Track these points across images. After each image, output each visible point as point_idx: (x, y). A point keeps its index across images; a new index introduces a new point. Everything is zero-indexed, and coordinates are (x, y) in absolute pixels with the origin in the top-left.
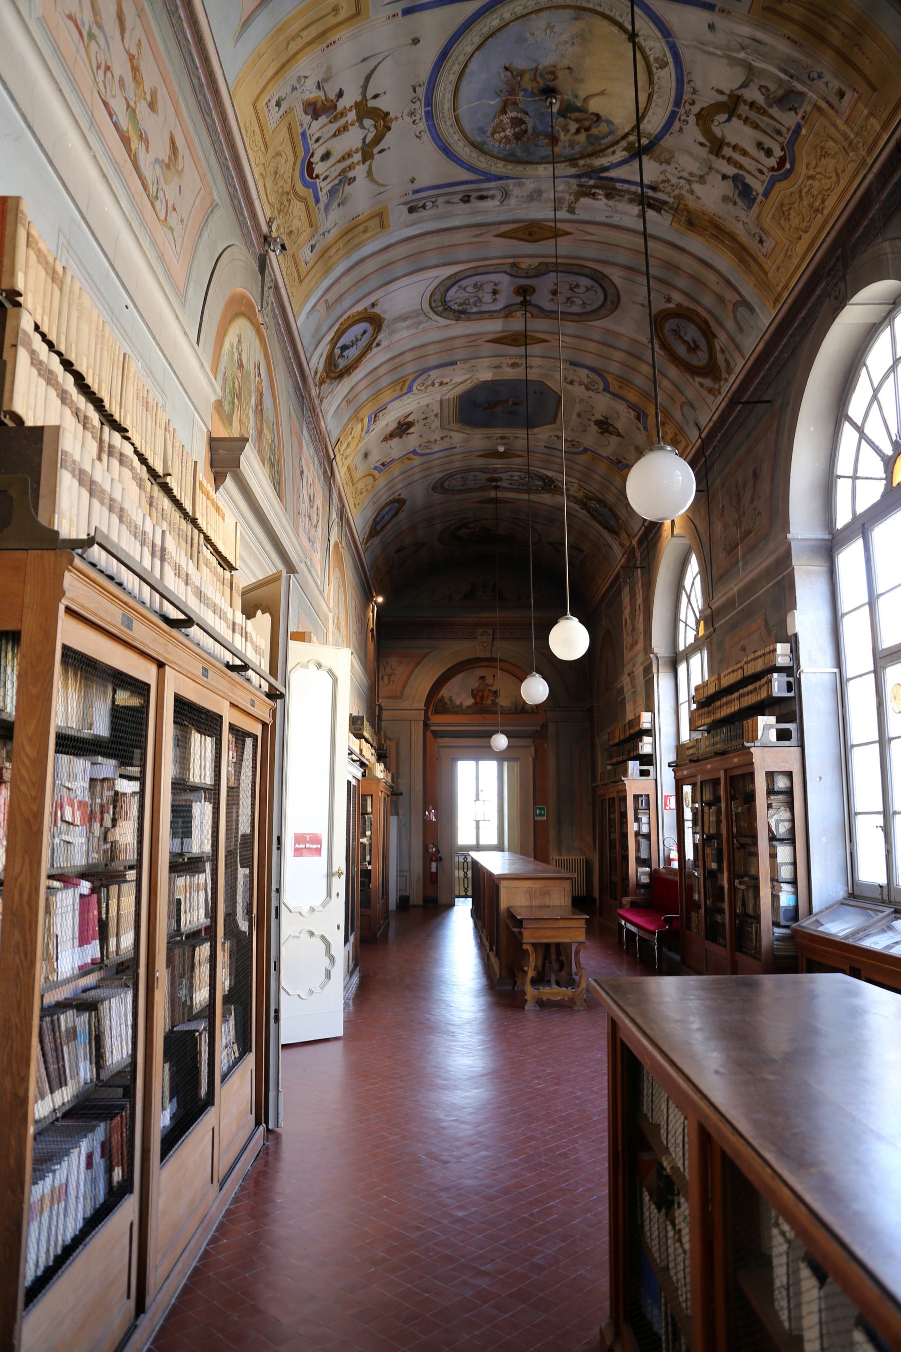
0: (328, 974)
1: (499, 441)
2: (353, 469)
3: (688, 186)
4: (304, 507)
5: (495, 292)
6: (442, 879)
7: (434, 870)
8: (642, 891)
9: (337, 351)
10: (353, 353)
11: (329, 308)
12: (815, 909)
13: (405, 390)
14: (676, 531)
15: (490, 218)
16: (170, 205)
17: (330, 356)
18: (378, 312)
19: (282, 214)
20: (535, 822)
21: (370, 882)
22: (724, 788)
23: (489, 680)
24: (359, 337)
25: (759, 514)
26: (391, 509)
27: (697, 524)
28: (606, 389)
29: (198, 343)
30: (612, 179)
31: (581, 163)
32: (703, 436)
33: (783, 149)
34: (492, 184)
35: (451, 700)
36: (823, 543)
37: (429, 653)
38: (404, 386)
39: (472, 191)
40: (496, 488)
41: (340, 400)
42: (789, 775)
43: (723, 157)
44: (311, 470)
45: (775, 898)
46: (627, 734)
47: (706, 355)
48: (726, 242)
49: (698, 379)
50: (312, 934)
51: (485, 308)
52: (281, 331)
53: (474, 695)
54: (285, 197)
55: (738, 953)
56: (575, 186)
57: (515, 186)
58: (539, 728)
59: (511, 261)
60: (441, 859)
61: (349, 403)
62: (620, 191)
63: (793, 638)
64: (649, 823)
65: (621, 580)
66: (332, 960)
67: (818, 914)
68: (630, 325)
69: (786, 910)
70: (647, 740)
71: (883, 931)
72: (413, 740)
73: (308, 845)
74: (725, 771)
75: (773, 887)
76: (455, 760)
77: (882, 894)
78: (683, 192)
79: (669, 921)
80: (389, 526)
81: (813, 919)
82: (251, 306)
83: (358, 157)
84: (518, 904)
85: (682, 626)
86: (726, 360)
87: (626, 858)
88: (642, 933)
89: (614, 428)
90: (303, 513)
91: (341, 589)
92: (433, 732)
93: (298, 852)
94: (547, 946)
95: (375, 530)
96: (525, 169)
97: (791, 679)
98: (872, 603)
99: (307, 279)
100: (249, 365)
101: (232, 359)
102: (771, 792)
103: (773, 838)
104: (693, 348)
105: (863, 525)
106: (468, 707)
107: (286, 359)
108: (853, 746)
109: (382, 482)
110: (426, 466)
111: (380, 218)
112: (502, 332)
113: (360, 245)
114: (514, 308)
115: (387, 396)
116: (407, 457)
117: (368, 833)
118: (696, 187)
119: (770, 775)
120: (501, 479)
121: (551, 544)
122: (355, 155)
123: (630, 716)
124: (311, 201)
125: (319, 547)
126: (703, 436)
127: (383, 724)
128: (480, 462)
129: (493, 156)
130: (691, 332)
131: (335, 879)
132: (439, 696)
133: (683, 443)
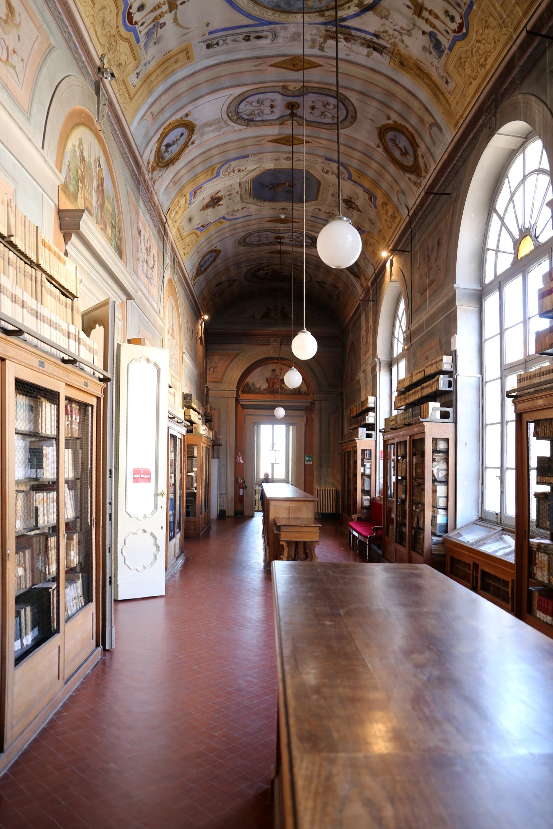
0: (155, 557)
1: (281, 211)
2: (181, 229)
3: (399, 36)
4: (142, 255)
5: (272, 107)
6: (246, 500)
7: (241, 494)
8: (365, 511)
9: (163, 148)
10: (174, 149)
11: (154, 117)
12: (458, 526)
13: (214, 175)
14: (393, 278)
15: (265, 53)
16: (11, 49)
17: (158, 151)
18: (190, 120)
19: (111, 52)
20: (305, 465)
21: (195, 501)
22: (410, 450)
23: (278, 372)
24: (178, 138)
25: (440, 269)
26: (211, 256)
27: (405, 273)
28: (350, 178)
29: (43, 148)
30: (348, 27)
31: (327, 14)
32: (410, 214)
33: (461, 18)
34: (265, 28)
35: (253, 385)
36: (476, 292)
37: (240, 353)
38: (213, 172)
39: (251, 32)
40: (280, 243)
41: (168, 182)
42: (447, 440)
43: (423, 18)
44: (147, 230)
45: (434, 518)
46: (360, 411)
47: (412, 159)
48: (425, 80)
49: (408, 175)
50: (145, 531)
51: (266, 117)
52: (117, 135)
53: (268, 381)
54: (112, 39)
55: (412, 552)
56: (323, 31)
57: (281, 29)
58: (309, 405)
59: (282, 84)
60: (246, 487)
61: (175, 183)
62: (354, 36)
63: (454, 353)
64: (371, 468)
65: (361, 308)
66: (158, 548)
67: (459, 529)
68: (363, 133)
69: (441, 526)
70: (371, 414)
71: (498, 540)
72: (229, 411)
73: (141, 475)
74: (410, 436)
75: (434, 512)
76: (259, 423)
77: (497, 519)
78: (397, 41)
79: (376, 530)
80: (210, 268)
81: (456, 532)
82: (89, 118)
83: (165, 8)
84: (281, 516)
85: (396, 340)
86: (425, 163)
87: (356, 489)
88: (360, 537)
89: (355, 205)
90: (141, 259)
91: (175, 310)
92: (242, 405)
93: (136, 480)
94: (297, 543)
95: (200, 270)
96: (287, 17)
97: (451, 379)
98: (501, 334)
99: (136, 97)
100: (90, 157)
101: (75, 155)
102: (435, 451)
103: (434, 481)
104: (404, 153)
105: (500, 282)
106: (264, 389)
107: (123, 154)
108: (487, 425)
109: (203, 238)
110: (233, 227)
111: (187, 52)
112: (279, 135)
113: (173, 72)
114: (286, 118)
115: (202, 179)
116: (219, 221)
117: (195, 469)
118: (405, 38)
119: (435, 440)
120: (283, 238)
121: (318, 282)
122: (163, 6)
123: (363, 399)
124: (133, 40)
125: (155, 282)
126: (410, 214)
127: (210, 399)
128: (269, 225)
129: (264, 7)
130: (403, 142)
131: (160, 498)
132: (246, 382)
133: (398, 219)
